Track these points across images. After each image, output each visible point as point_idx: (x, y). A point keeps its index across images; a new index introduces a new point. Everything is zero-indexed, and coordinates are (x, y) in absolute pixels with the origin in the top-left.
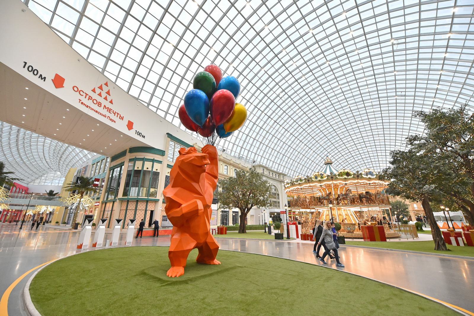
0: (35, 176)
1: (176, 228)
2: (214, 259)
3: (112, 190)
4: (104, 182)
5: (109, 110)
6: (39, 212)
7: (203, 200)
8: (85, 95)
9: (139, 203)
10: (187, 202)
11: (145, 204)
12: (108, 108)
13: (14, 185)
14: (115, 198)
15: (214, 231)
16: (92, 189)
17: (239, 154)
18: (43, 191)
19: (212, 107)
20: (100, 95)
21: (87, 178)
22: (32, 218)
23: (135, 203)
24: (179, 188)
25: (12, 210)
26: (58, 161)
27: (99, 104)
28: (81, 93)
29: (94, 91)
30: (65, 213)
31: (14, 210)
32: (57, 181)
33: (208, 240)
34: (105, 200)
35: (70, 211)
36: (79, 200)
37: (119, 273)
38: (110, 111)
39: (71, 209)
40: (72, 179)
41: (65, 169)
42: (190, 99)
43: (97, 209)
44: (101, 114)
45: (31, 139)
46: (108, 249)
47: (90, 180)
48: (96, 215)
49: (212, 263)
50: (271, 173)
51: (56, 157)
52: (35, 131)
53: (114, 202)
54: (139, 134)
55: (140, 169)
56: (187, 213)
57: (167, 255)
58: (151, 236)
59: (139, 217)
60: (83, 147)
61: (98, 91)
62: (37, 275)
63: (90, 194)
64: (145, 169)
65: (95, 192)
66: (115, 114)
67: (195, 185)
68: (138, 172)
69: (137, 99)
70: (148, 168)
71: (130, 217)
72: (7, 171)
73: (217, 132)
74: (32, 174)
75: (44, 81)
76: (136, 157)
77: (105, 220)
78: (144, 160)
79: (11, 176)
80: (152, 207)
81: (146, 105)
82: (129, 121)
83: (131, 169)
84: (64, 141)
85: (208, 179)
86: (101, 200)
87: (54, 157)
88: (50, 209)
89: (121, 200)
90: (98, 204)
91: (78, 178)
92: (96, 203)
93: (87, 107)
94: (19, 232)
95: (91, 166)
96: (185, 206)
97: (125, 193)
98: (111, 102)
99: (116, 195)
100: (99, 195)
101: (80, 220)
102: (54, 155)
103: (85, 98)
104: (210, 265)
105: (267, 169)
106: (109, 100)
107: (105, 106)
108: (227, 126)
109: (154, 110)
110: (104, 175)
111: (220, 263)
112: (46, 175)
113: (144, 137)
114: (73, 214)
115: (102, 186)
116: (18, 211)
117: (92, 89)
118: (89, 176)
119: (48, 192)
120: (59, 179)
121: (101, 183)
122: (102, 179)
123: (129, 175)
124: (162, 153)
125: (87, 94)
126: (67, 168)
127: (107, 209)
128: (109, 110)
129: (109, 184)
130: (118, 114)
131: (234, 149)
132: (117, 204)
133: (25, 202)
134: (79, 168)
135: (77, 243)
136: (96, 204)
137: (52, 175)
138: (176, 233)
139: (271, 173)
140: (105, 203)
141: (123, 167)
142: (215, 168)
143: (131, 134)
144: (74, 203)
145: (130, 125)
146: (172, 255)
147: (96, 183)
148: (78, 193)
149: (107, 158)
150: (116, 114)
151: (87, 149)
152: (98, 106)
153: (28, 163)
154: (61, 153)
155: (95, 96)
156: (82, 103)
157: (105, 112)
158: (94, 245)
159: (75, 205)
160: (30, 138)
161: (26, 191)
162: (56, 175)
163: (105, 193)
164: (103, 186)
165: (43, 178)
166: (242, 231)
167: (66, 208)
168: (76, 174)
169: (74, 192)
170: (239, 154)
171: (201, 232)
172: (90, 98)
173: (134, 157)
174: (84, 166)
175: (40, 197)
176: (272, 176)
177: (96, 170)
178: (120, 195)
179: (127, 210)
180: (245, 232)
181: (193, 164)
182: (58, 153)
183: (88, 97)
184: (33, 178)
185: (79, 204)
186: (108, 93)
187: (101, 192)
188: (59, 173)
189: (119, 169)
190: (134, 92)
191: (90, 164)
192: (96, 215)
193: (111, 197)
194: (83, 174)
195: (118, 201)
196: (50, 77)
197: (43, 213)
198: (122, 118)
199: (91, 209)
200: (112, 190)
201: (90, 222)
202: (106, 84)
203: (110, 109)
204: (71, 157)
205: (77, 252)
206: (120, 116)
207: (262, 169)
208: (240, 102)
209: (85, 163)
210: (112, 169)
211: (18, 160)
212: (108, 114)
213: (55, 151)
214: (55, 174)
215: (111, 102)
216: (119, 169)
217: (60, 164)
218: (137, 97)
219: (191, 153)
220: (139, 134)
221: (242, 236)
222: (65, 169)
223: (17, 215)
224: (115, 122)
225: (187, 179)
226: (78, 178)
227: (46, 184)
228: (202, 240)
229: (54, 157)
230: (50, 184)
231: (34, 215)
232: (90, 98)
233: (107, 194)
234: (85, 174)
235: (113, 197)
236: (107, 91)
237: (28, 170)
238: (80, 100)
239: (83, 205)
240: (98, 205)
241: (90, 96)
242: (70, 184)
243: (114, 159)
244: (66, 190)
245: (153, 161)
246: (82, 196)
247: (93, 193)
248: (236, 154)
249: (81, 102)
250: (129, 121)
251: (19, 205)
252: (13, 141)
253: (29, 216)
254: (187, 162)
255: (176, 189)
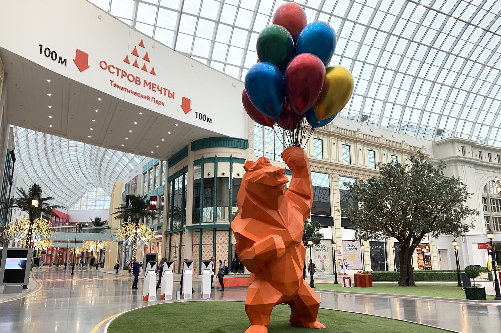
0: (74, 197)
1: (254, 275)
2: (315, 321)
3: (177, 214)
4: (163, 201)
5: (152, 86)
6: (88, 250)
7: (285, 233)
8: (116, 71)
9: (218, 234)
10: (262, 238)
11: (228, 234)
12: (150, 83)
13: (54, 214)
14: (182, 225)
15: (347, 281)
16: (148, 214)
17: (400, 121)
18: (88, 218)
19: (293, 81)
20: (136, 65)
21: (140, 197)
22: (80, 259)
23: (212, 233)
24: (250, 219)
25: (56, 248)
26: (97, 172)
27: (137, 80)
28: (111, 68)
29: (127, 61)
30: (120, 251)
31: (58, 249)
32: (101, 203)
33: (301, 293)
34: (169, 228)
35: (126, 249)
36: (134, 231)
37: (192, 329)
38: (153, 87)
39: (127, 245)
40: (120, 201)
41: (109, 183)
42: (254, 81)
43: (160, 244)
44: (141, 96)
45: (60, 144)
46: (180, 303)
47: (143, 199)
48: (160, 253)
49: (311, 326)
50: (485, 154)
51: (94, 166)
52: (66, 136)
53: (181, 233)
54: (202, 117)
55: (212, 176)
56: (260, 255)
57: (244, 310)
58: (488, 316)
59: (220, 255)
60: (126, 150)
61: (132, 59)
62: (110, 326)
63: (148, 221)
64: (219, 175)
65: (154, 218)
66: (161, 91)
67: (273, 214)
68: (209, 182)
69: (189, 56)
70: (223, 174)
71: (208, 255)
72: (45, 197)
73: (307, 119)
74: (70, 195)
75: (66, 65)
76: (203, 157)
77: (171, 263)
78: (216, 160)
79: (51, 203)
80: (208, 250)
81: (205, 62)
82: (184, 98)
83: (198, 177)
84: (100, 145)
85: (295, 202)
86: (164, 230)
87: (92, 166)
88: (100, 246)
89: (192, 230)
90: (160, 236)
91: (128, 197)
92: (158, 234)
93: (122, 89)
94: (72, 279)
95: (142, 176)
96: (259, 245)
97: (197, 217)
98: (153, 72)
99: (184, 221)
100: (159, 221)
101: (140, 259)
102: (91, 164)
103: (118, 75)
104: (309, 328)
105: (473, 145)
106: (149, 70)
107: (145, 81)
108: (320, 110)
109: (220, 67)
110: (161, 190)
111: (325, 327)
112: (86, 195)
113: (210, 121)
114: (130, 252)
115: (162, 208)
116: (63, 249)
117: (124, 59)
118: (141, 194)
119: (94, 220)
120: (103, 199)
121: (160, 204)
122: (160, 196)
123: (197, 185)
124: (243, 144)
125: (118, 70)
126: (111, 182)
127: (173, 244)
128: (152, 86)
129: (171, 204)
130: (165, 90)
131: (387, 113)
132: (187, 236)
133: (70, 236)
134: (126, 182)
135: (142, 294)
136: (157, 237)
137: (94, 193)
138: (254, 281)
139: (485, 154)
140: (169, 234)
141: (186, 174)
142: (304, 183)
143: (190, 119)
144: (129, 237)
145: (186, 105)
146: (249, 310)
147: (153, 203)
148: (132, 221)
149: (162, 161)
150: (163, 90)
151: (132, 152)
152: (136, 83)
153: (62, 179)
154: (99, 160)
155: (129, 69)
156: (115, 85)
157: (146, 91)
158: (163, 298)
159: (131, 239)
160: (59, 142)
161: (66, 219)
162: (98, 194)
163: (168, 218)
164: (163, 206)
165: (83, 199)
166: (404, 281)
167: (120, 243)
168: (123, 190)
169: (126, 220)
170: (400, 121)
171: (287, 280)
172: (124, 74)
173: (200, 157)
174: (133, 177)
175: (81, 227)
176: (487, 160)
177: (149, 180)
178: (189, 222)
179: (201, 244)
180: (413, 285)
181: (264, 184)
182: (96, 160)
183: (120, 72)
184: (72, 200)
185: (135, 237)
186: (146, 58)
187: (161, 216)
188: (101, 189)
189: (181, 177)
190: (184, 45)
191: (141, 173)
192: (160, 253)
193: (177, 224)
194: (133, 192)
195: (186, 230)
196: (71, 57)
197: (92, 252)
198: (172, 96)
199: (152, 245)
200: (177, 214)
201: (152, 265)
202: (141, 45)
203: (153, 84)
204: (113, 164)
205: (143, 305)
206: (169, 93)
207: (458, 147)
208: (339, 64)
209: (134, 171)
210: (172, 179)
211: (51, 176)
212: (151, 94)
213: (92, 158)
214: (97, 191)
215: (153, 72)
216: (181, 177)
217: (101, 176)
218: (189, 53)
219: (260, 168)
220: (202, 117)
221: (408, 293)
222: (109, 183)
223: (63, 255)
224: (163, 104)
225: (259, 206)
226: (128, 197)
227: (88, 208)
228: (291, 292)
229: (92, 166)
230: (93, 208)
231: (82, 254)
232: (124, 74)
233: (170, 219)
234: (135, 189)
235: (179, 223)
236: (143, 56)
237: (64, 189)
238: (112, 81)
239: (140, 239)
240: (161, 238)
241: (123, 72)
242: (119, 208)
243: (172, 162)
244: (116, 218)
245: (230, 160)
246: (137, 225)
247: (151, 219)
248: (392, 122)
249: (113, 83)
250: (184, 98)
251: (63, 242)
252: (41, 150)
253: (77, 257)
254: (257, 183)
255: (247, 221)
